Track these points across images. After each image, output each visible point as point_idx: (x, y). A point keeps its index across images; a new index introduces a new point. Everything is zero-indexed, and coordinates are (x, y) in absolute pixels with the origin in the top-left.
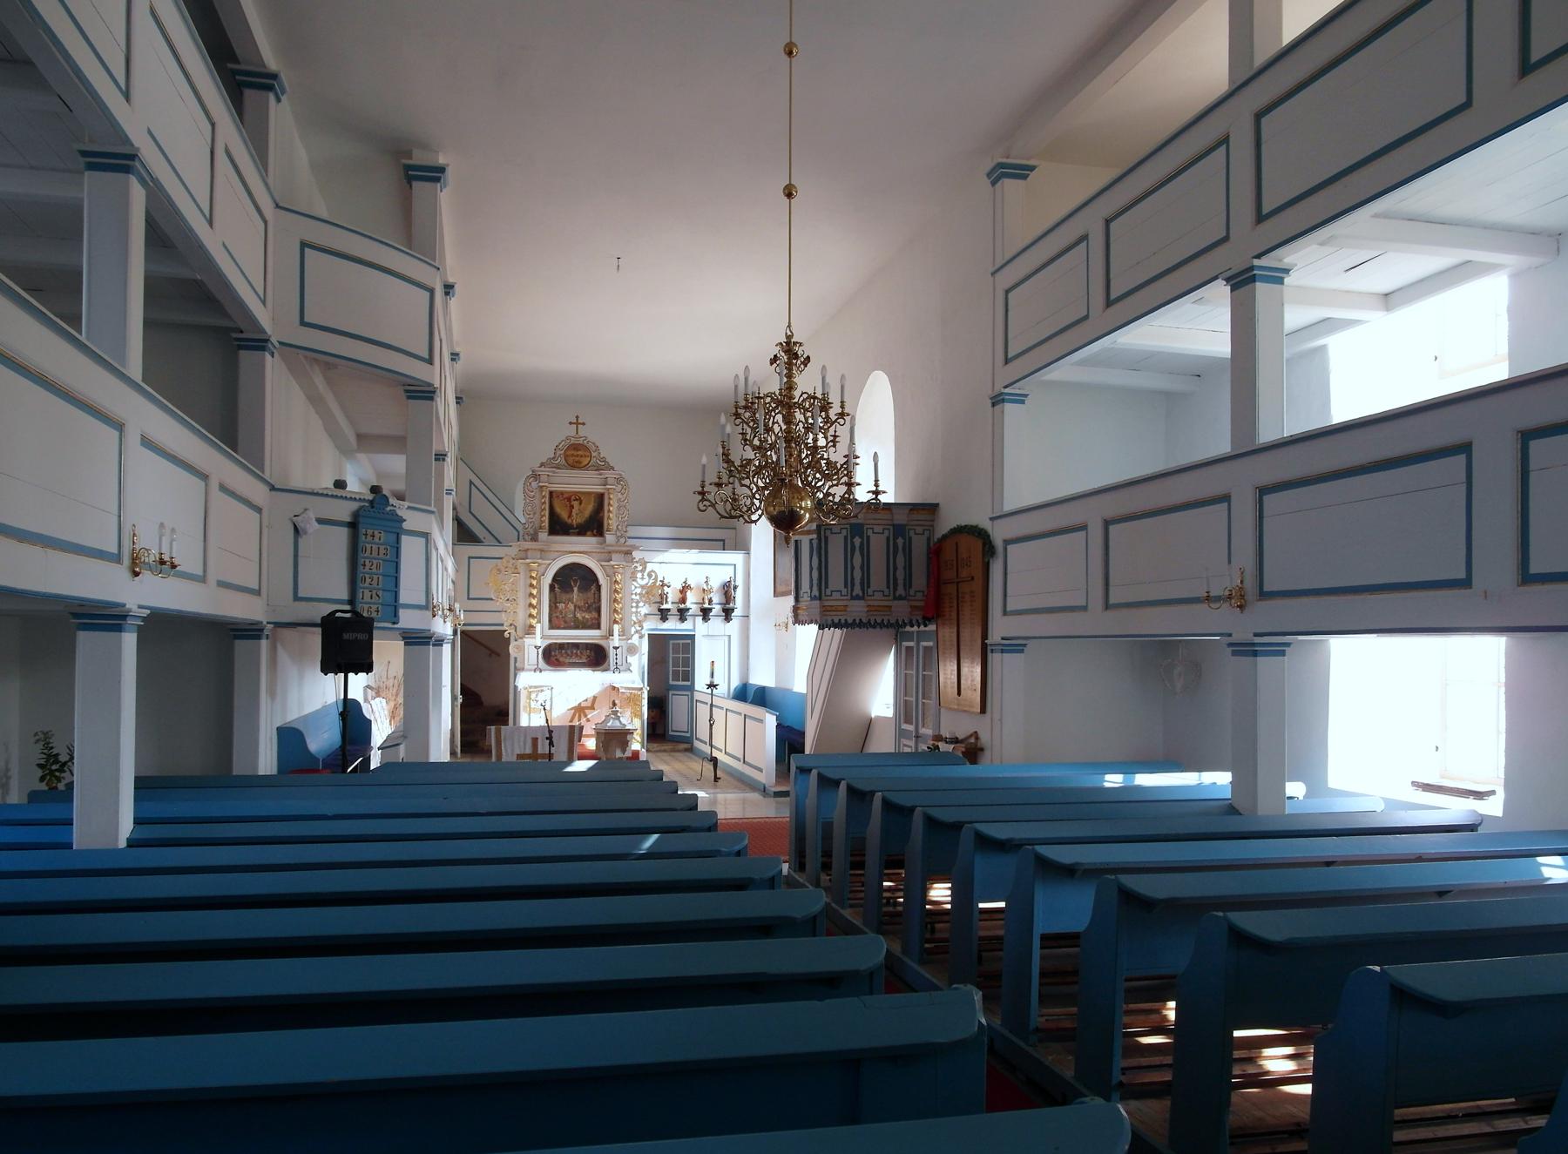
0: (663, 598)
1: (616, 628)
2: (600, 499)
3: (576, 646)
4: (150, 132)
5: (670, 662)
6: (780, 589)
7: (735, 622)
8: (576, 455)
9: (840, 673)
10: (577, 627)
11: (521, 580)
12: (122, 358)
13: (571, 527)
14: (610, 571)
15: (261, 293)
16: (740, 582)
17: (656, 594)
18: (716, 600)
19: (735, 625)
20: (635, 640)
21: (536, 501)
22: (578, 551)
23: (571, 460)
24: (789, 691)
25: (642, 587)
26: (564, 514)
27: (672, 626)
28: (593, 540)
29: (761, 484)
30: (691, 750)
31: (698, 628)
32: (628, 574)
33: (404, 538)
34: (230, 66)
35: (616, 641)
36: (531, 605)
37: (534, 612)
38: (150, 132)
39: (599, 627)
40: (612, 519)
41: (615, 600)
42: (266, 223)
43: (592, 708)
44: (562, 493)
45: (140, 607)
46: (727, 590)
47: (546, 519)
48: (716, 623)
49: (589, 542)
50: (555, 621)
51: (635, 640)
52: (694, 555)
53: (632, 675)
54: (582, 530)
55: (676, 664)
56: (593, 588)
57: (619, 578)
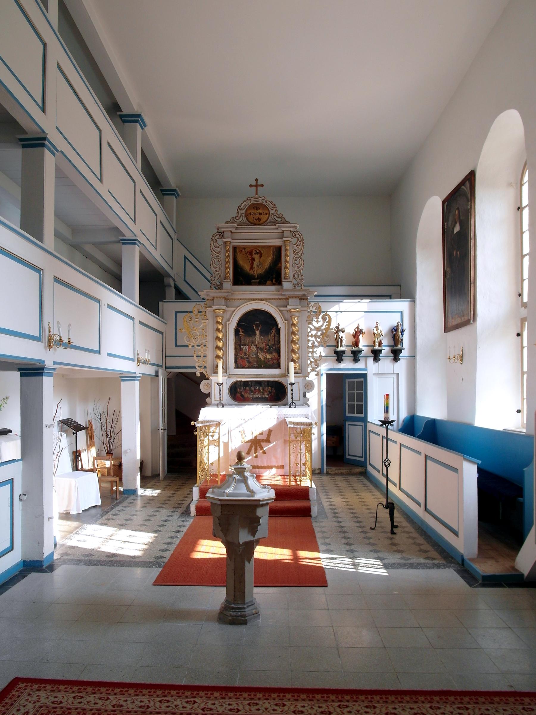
0: (338, 341)
1: (292, 365)
2: (278, 251)
3: (259, 383)
5: (346, 397)
6: (452, 322)
7: (402, 363)
8: (256, 213)
9: (72, 410)
10: (259, 367)
11: (210, 325)
13: (253, 277)
14: (287, 315)
16: (406, 326)
17: (332, 339)
18: (385, 342)
19: (401, 366)
20: (312, 377)
21: (222, 256)
22: (258, 298)
23: (251, 218)
24: (471, 427)
26: (246, 267)
28: (273, 288)
30: (365, 474)
31: (371, 368)
32: (305, 318)
33: (368, 423)
34: (119, 113)
35: (292, 378)
36: (218, 347)
37: (220, 353)
40: (289, 268)
41: (293, 341)
42: (172, 239)
43: (268, 441)
44: (244, 248)
46: (395, 334)
47: (231, 271)
48: (386, 364)
49: (268, 290)
50: (240, 361)
51: (312, 377)
52: (364, 304)
53: (310, 410)
54: (262, 280)
55: (351, 399)
56: (273, 331)
57: (295, 321)
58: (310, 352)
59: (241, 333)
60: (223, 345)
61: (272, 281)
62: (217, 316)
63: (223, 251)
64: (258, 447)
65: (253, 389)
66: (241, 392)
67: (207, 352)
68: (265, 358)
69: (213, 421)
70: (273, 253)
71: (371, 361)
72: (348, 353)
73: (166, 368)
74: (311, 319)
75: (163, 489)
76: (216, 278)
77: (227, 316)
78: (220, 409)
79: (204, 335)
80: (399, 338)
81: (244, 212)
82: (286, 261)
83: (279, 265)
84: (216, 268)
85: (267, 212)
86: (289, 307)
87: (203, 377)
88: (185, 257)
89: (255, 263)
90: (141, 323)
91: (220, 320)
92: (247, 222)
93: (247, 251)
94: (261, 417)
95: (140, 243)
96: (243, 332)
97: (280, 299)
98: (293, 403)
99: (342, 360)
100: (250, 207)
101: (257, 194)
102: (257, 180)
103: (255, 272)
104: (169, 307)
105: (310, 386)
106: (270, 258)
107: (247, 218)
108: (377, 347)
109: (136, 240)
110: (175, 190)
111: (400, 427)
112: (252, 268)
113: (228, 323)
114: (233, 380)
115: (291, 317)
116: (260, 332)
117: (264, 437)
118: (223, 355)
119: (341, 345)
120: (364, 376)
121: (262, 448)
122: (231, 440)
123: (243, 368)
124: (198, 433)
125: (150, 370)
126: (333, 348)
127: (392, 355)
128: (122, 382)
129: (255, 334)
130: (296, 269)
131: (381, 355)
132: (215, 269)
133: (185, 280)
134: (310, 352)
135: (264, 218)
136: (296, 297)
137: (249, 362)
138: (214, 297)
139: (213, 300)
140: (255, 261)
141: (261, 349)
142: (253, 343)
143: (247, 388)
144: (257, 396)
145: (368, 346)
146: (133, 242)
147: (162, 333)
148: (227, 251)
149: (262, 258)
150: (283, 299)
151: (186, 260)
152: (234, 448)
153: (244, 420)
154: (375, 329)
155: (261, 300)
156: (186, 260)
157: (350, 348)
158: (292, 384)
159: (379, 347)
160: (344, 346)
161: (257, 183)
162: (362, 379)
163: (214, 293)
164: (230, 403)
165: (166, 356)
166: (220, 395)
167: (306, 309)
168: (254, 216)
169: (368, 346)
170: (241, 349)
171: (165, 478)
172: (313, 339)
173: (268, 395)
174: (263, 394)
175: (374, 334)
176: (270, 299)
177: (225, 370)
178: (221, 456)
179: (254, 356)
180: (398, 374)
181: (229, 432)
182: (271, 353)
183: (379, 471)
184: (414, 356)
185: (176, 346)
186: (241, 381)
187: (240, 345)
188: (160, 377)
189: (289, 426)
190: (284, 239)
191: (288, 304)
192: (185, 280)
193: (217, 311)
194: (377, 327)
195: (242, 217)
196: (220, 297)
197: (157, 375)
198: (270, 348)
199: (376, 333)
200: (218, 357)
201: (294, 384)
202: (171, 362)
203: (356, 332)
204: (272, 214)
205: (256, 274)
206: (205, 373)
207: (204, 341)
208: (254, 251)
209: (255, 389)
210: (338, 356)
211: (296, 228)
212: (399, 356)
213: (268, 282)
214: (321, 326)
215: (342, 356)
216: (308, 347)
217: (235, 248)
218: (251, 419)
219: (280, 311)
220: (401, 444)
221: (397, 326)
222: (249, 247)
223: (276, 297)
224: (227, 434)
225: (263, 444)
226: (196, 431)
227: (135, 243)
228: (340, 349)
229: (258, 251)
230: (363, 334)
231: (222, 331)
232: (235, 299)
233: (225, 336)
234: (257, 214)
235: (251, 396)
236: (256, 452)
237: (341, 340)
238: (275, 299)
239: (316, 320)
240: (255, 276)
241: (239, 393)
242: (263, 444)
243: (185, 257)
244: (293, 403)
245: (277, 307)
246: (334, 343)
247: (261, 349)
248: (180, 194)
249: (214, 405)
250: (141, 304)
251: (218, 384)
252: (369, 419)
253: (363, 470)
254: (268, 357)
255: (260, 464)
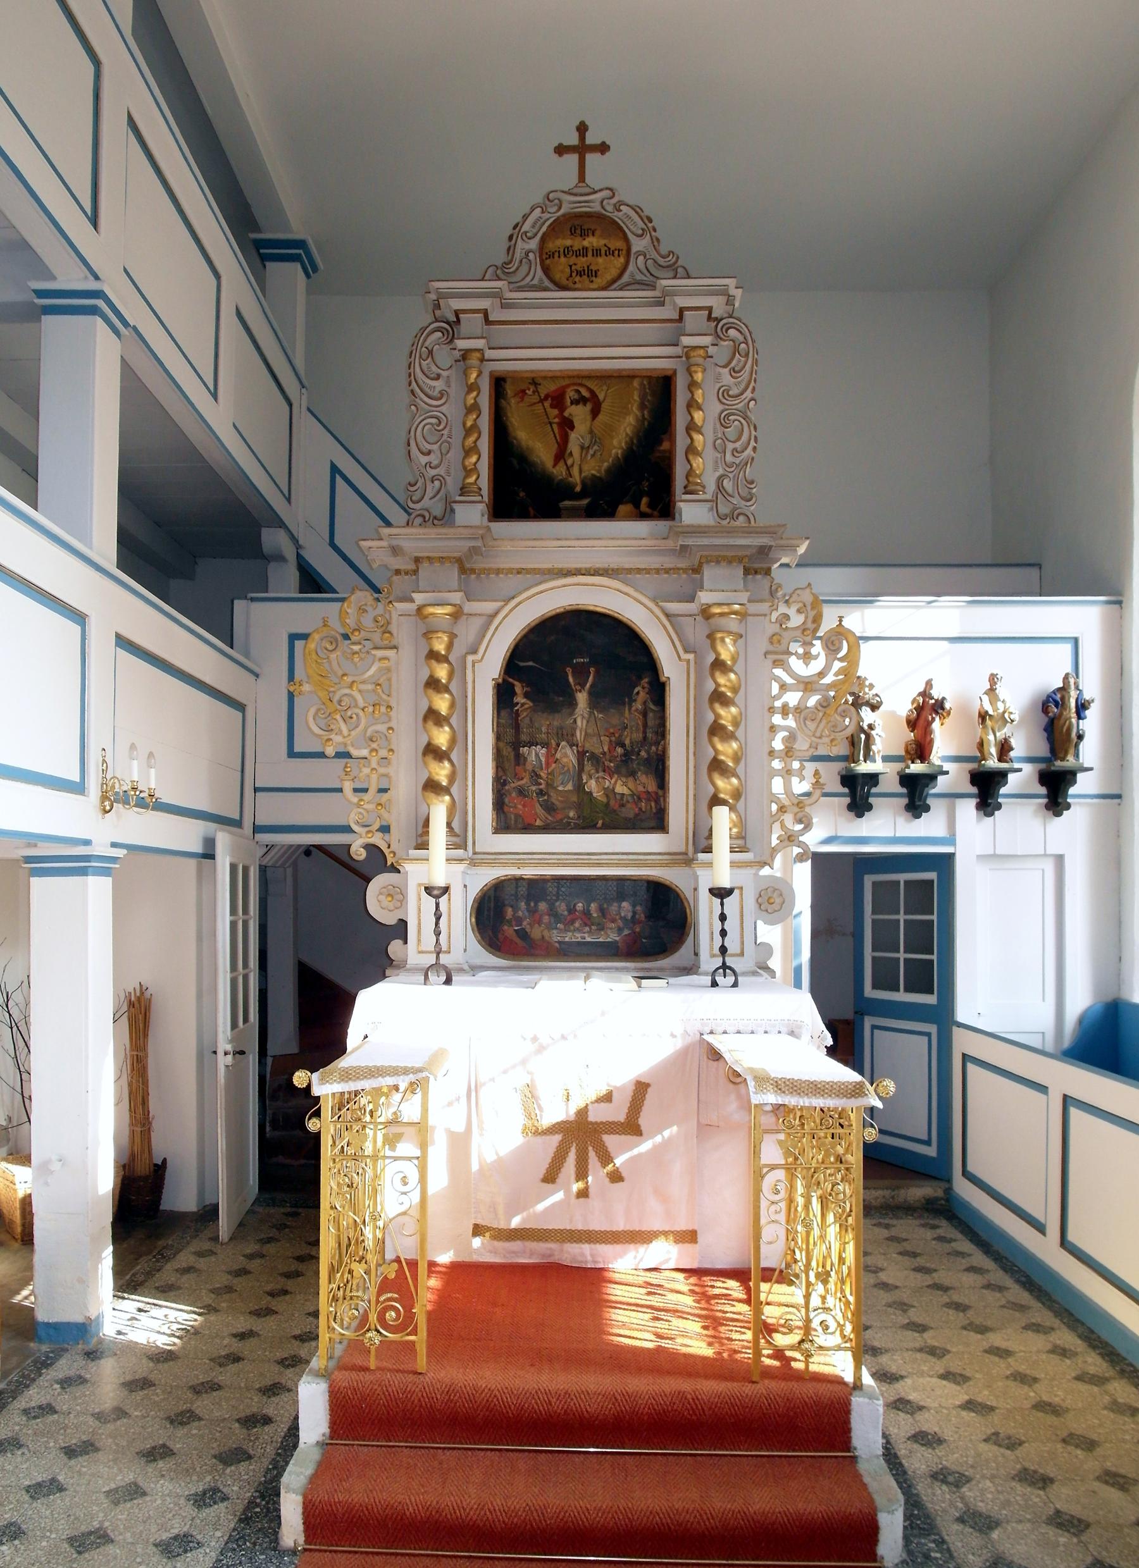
0: (860, 741)
1: (722, 819)
2: (660, 392)
4: (125, 270)
7: (1079, 816)
8: (582, 245)
10: (586, 825)
11: (404, 667)
12: (86, 539)
13: (565, 490)
15: (286, 492)
16: (1091, 685)
18: (1019, 748)
22: (587, 567)
25: (807, 685)
26: (542, 452)
27: (885, 829)
28: (642, 527)
29: (125, 1444)
32: (759, 643)
35: (721, 868)
37: (441, 772)
38: (125, 270)
39: (658, 822)
40: (702, 454)
41: (716, 730)
42: (291, 405)
43: (631, 1127)
45: (114, 845)
46: (1056, 717)
48: (1020, 819)
49: (622, 538)
52: (950, 613)
54: (601, 500)
55: (885, 939)
56: (641, 694)
57: (727, 650)
58: (776, 773)
59: (519, 699)
60: (453, 741)
61: (637, 505)
62: (428, 634)
63: (456, 390)
64: (592, 1154)
65: (561, 907)
66: (519, 921)
67: (390, 770)
68: (609, 792)
69: (395, 1071)
70: (643, 398)
71: (967, 809)
72: (890, 782)
73: (257, 829)
74: (783, 647)
75: (210, 1310)
76: (430, 492)
77: (467, 631)
78: (436, 990)
79: (381, 706)
80: (1069, 730)
81: (534, 244)
82: (691, 427)
83: (665, 445)
84: (429, 453)
85: (620, 244)
86: (704, 597)
87: (379, 861)
88: (335, 470)
89: (573, 436)
90: (123, 642)
91: (440, 647)
92: (547, 283)
93: (543, 392)
94: (598, 1028)
95: (126, 324)
96: (526, 695)
97: (667, 571)
98: (724, 966)
99: (869, 807)
100: (556, 228)
101: (582, 177)
102: (582, 129)
103: (575, 471)
104: (268, 619)
105: (778, 900)
106: (631, 419)
107: (546, 270)
108: (993, 763)
109: (98, 294)
110: (301, 244)
111: (1067, 1043)
112: (561, 455)
113: (470, 658)
114: (486, 876)
115: (711, 637)
116: (590, 693)
117: (617, 1113)
118: (452, 778)
119: (868, 757)
120: (944, 864)
121: (606, 1158)
122: (481, 1128)
123: (527, 828)
124: (324, 1125)
125: (186, 836)
126: (839, 766)
127: (1043, 790)
128: (35, 881)
129: (572, 704)
130: (729, 458)
131: (1003, 791)
132: (424, 460)
133: (332, 544)
134: (776, 773)
135: (609, 266)
136: (730, 561)
137: (549, 808)
138: (417, 560)
139: (415, 572)
140: (572, 428)
141: (595, 759)
142: (566, 735)
143: (543, 906)
144: (578, 937)
145: (957, 759)
146: (85, 303)
147: (240, 707)
148: (472, 388)
149: (601, 417)
150: (676, 570)
151: (338, 478)
152: (490, 1158)
153: (535, 1039)
154: (986, 698)
155: (596, 572)
156: (338, 478)
157: (898, 766)
158: (721, 893)
159: (1000, 760)
160: (878, 759)
161: (582, 138)
162: (932, 875)
163: (417, 540)
164: (478, 961)
165: (256, 790)
166: (438, 934)
167: (764, 607)
168: (573, 260)
169: (957, 759)
170: (519, 759)
171: (241, 1229)
172: (791, 722)
173: (620, 930)
174: (601, 928)
175: (983, 716)
176: (629, 571)
177: (458, 838)
178: (431, 1190)
179: (570, 787)
180: (1059, 859)
181: (472, 1091)
182: (632, 774)
183: (1040, 1228)
184: (1119, 797)
185: (292, 754)
186: (518, 880)
187: (516, 745)
188: (223, 861)
189: (756, 1099)
190: (686, 341)
191: (702, 588)
192: (332, 544)
193: (431, 610)
194: (991, 691)
195: (524, 269)
196: (442, 560)
197: (209, 855)
198: (626, 754)
199: (991, 712)
200: (432, 786)
201: (729, 892)
202: (272, 810)
203: (920, 709)
204: (639, 253)
205: (576, 478)
206: (383, 846)
207: (382, 728)
208: (570, 394)
209: (572, 910)
210: (853, 794)
211: (730, 300)
212: (1066, 795)
213: (623, 509)
214: (822, 674)
215: (868, 795)
216: (772, 753)
217: (499, 383)
218: (564, 1037)
219: (667, 615)
220: (1065, 1097)
221: (1064, 690)
222: (553, 377)
223: (654, 562)
224: (464, 1100)
225: (610, 1140)
226: (317, 1114)
227: (93, 311)
228: (864, 767)
229: (585, 393)
230: (942, 718)
231: (446, 689)
232: (498, 571)
233: (460, 705)
234: (584, 252)
235: (555, 936)
236: (581, 1174)
237: (868, 737)
238: (648, 571)
239: (801, 651)
240: (574, 486)
241: (509, 922)
242: (611, 1141)
243: (335, 470)
244: (724, 966)
245: (654, 600)
246: (843, 749)
247: (595, 759)
248: (321, 266)
249: (415, 970)
250: (121, 565)
251: (428, 890)
252: (963, 1014)
253: (940, 1193)
254: (620, 789)
255: (597, 1224)
